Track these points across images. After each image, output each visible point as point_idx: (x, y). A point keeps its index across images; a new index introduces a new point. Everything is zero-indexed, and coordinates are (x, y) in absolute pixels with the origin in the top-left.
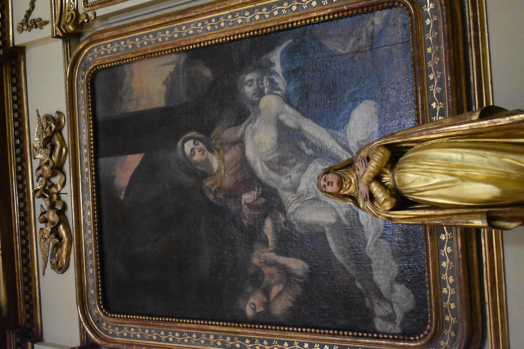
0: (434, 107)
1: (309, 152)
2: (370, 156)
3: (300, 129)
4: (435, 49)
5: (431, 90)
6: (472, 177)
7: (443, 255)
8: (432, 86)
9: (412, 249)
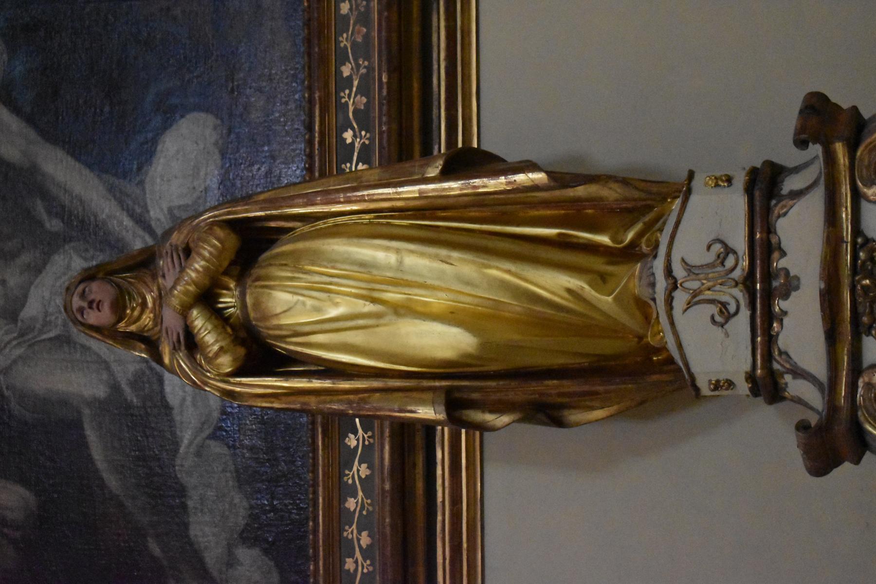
0: (349, 141)
1: (54, 225)
2: (192, 245)
3: (34, 170)
4: (357, 6)
5: (343, 101)
6: (420, 309)
7: (350, 481)
8: (347, 92)
9: (283, 466)
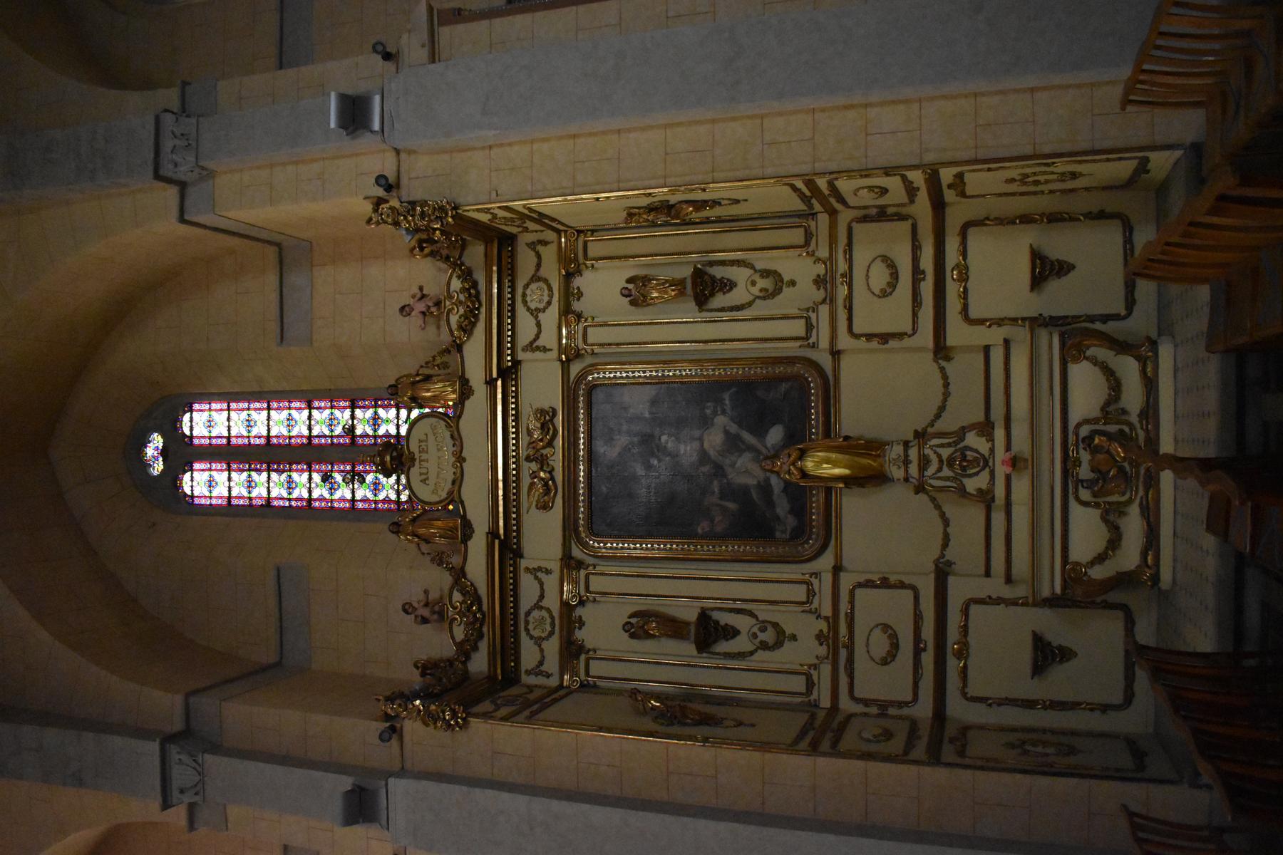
2: (390, 66)
